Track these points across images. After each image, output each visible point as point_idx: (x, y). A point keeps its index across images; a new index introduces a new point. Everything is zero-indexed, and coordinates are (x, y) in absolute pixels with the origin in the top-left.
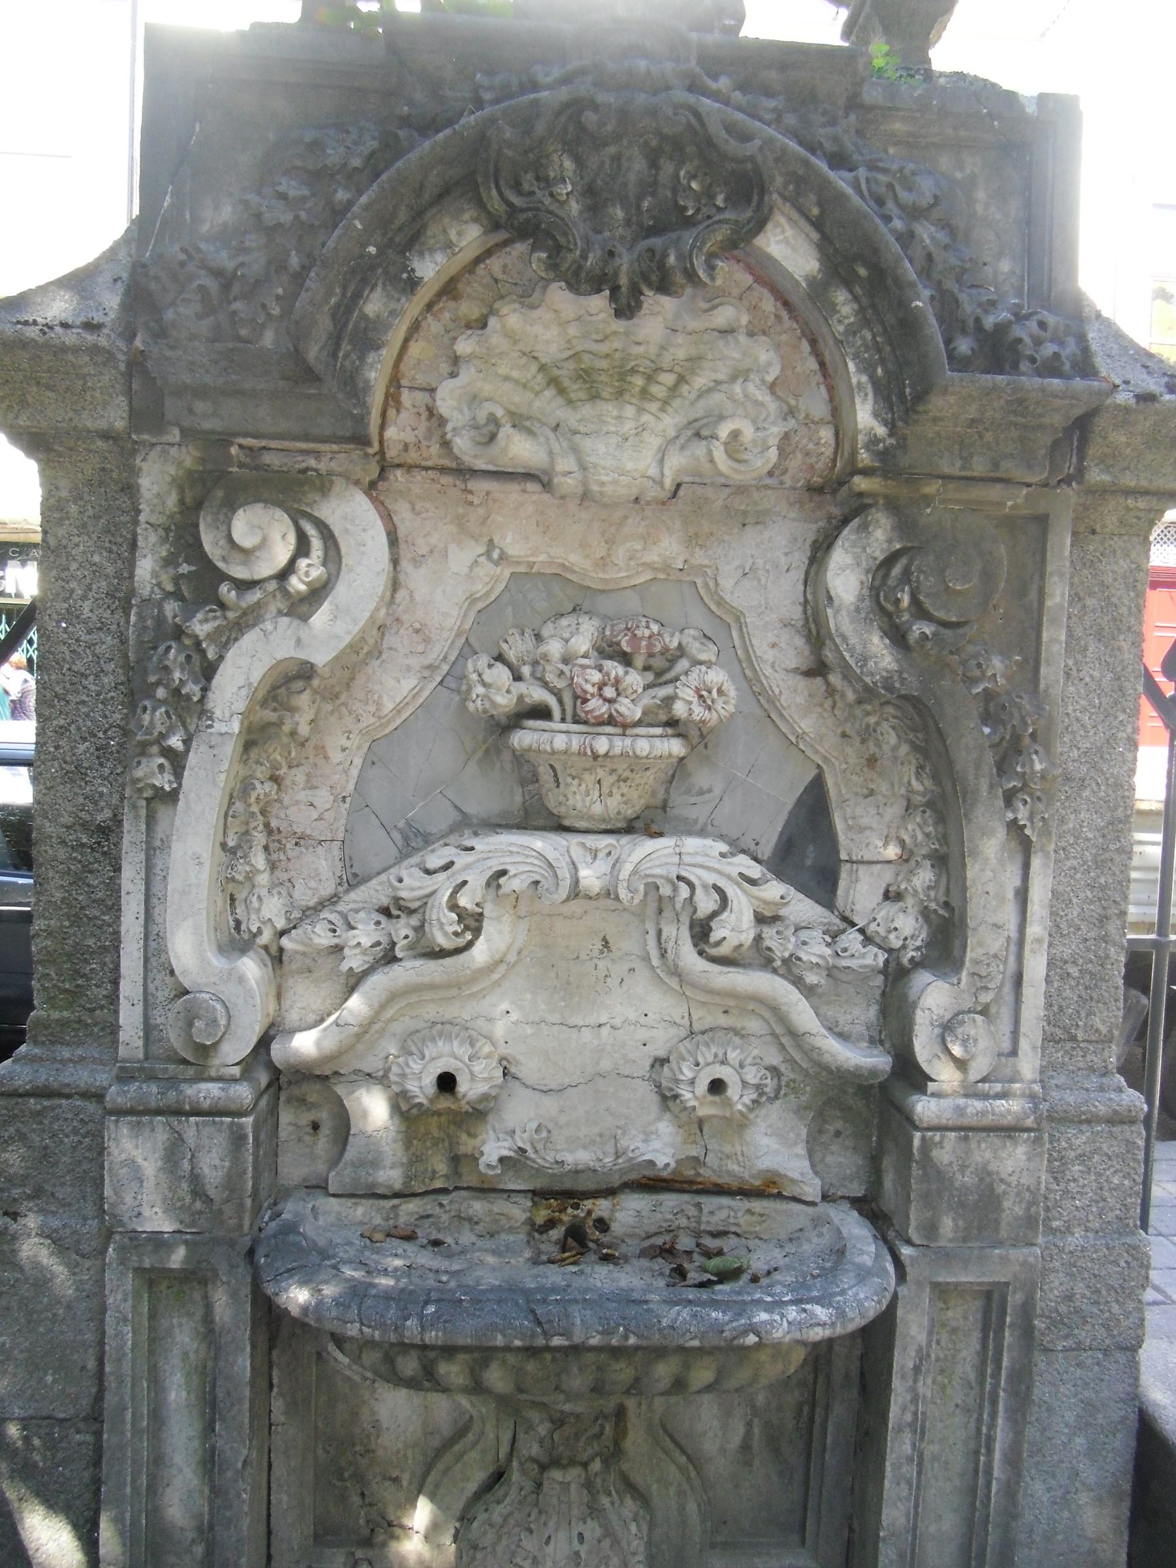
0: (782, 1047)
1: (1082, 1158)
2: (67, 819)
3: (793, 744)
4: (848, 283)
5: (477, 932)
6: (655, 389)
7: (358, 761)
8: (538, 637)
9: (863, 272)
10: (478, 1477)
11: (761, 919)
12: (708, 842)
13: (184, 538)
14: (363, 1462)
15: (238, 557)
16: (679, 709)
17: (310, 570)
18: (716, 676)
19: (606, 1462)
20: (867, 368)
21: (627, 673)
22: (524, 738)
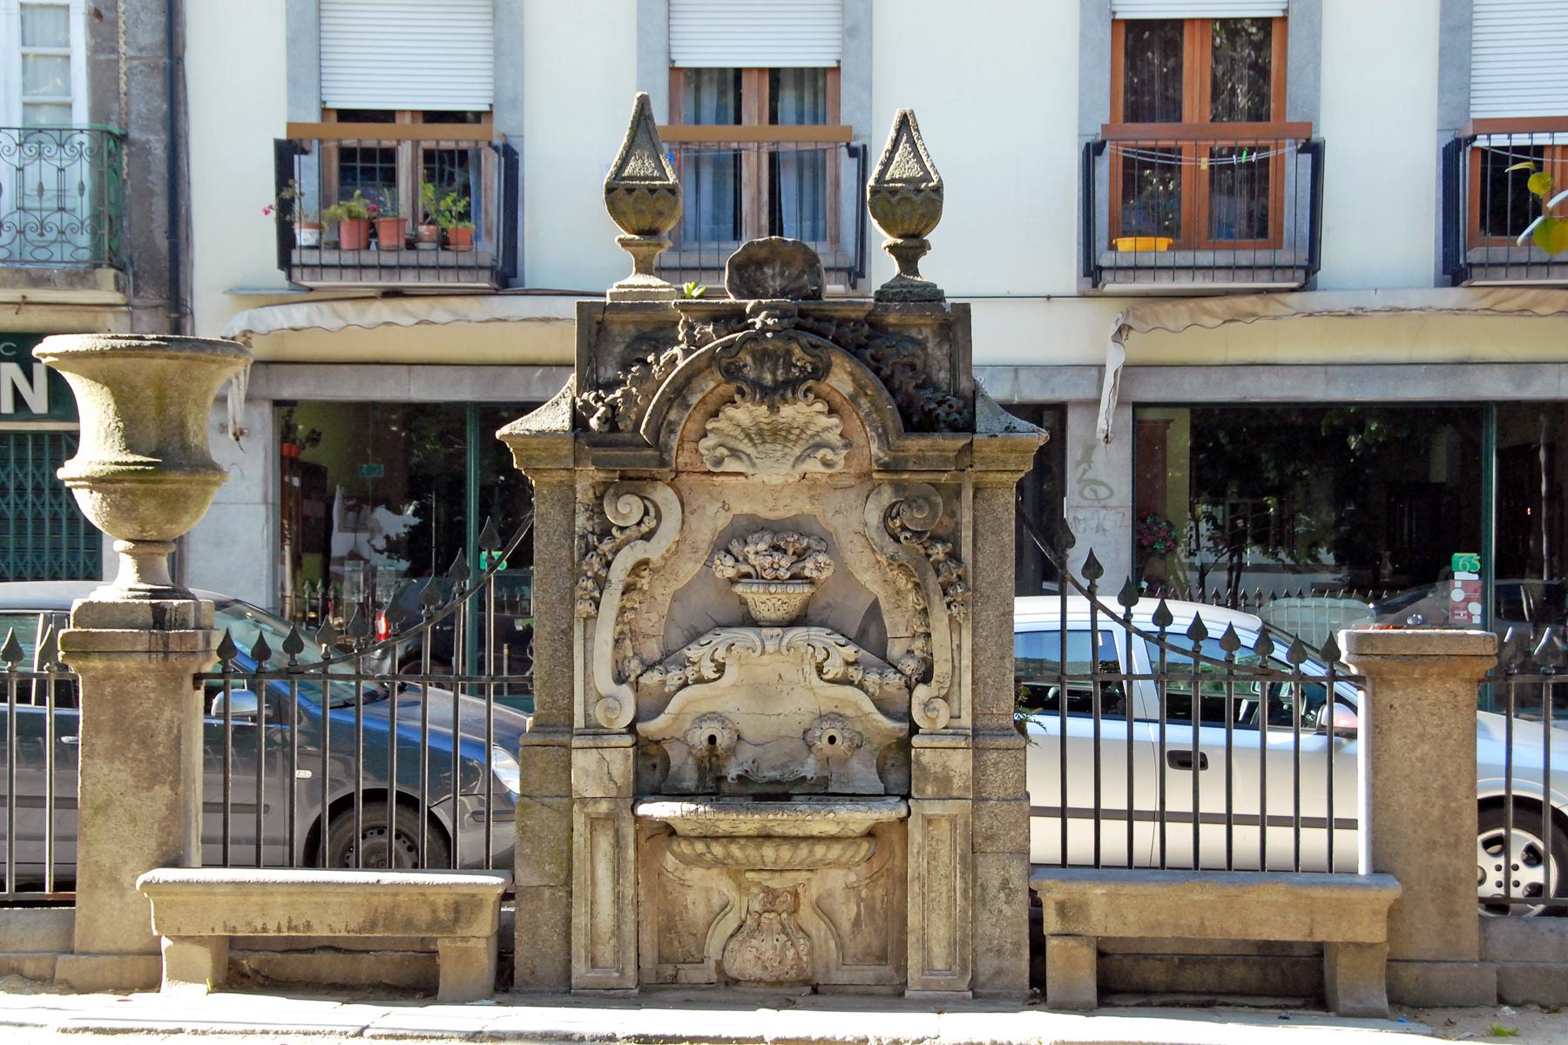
13: (597, 510)
17: (649, 523)
19: (790, 914)
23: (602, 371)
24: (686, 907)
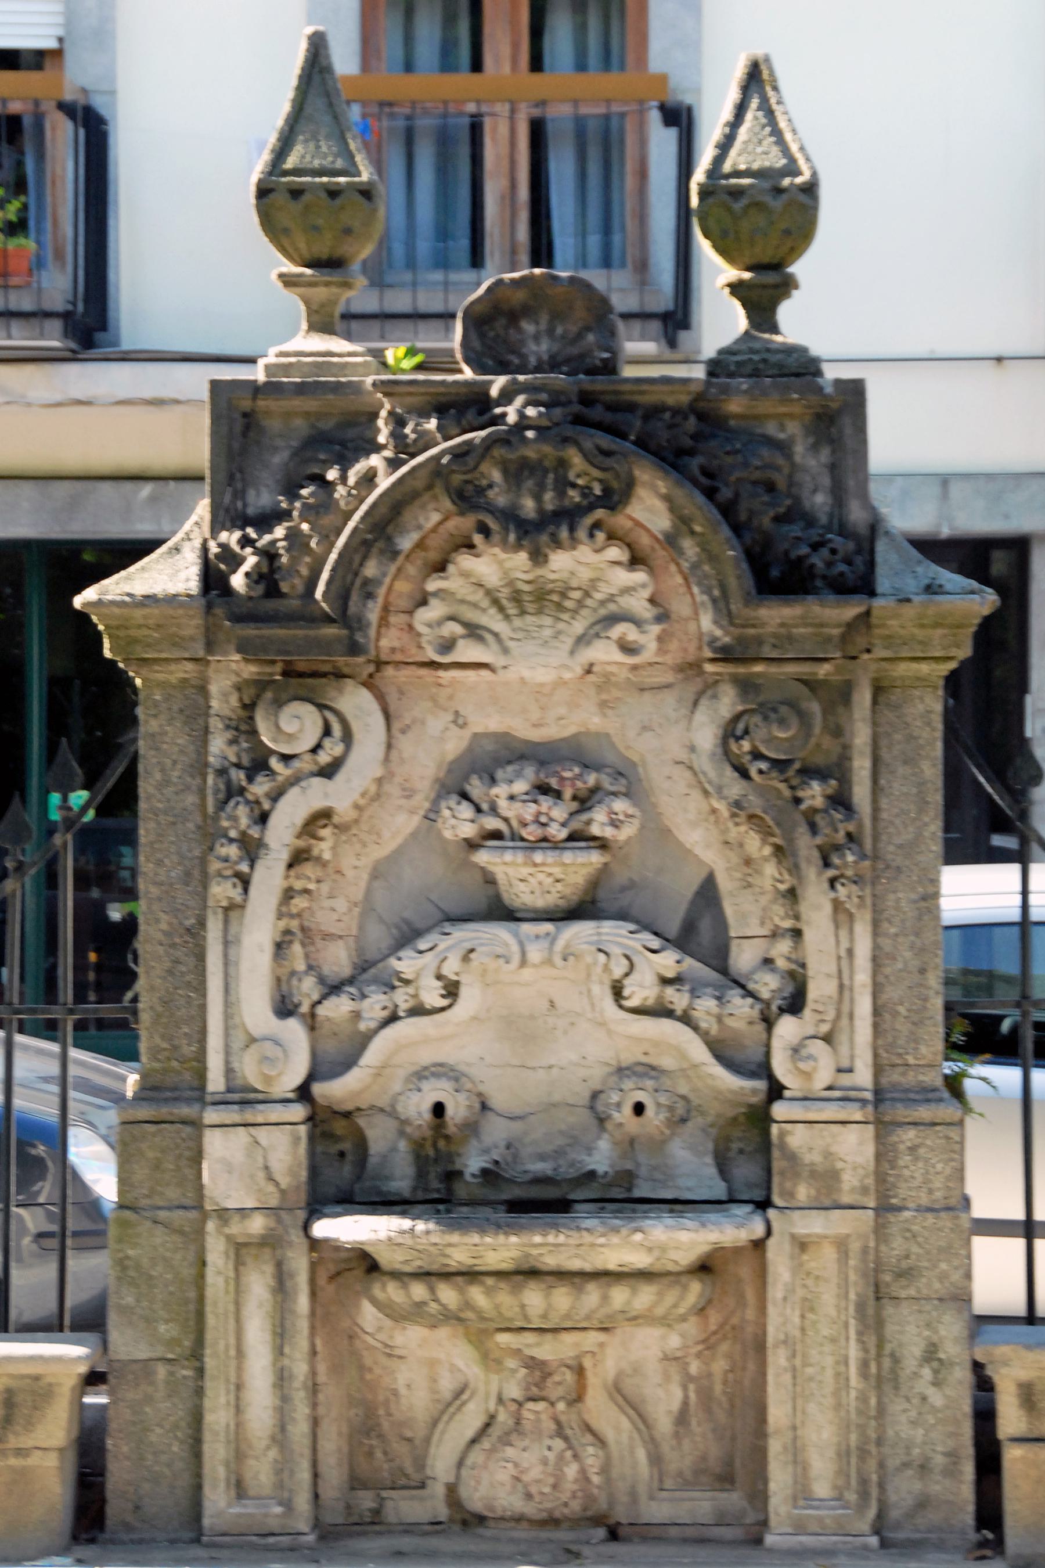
13: (244, 728)
17: (333, 749)
21: (316, 763)
23: (251, 495)
24: (395, 1393)
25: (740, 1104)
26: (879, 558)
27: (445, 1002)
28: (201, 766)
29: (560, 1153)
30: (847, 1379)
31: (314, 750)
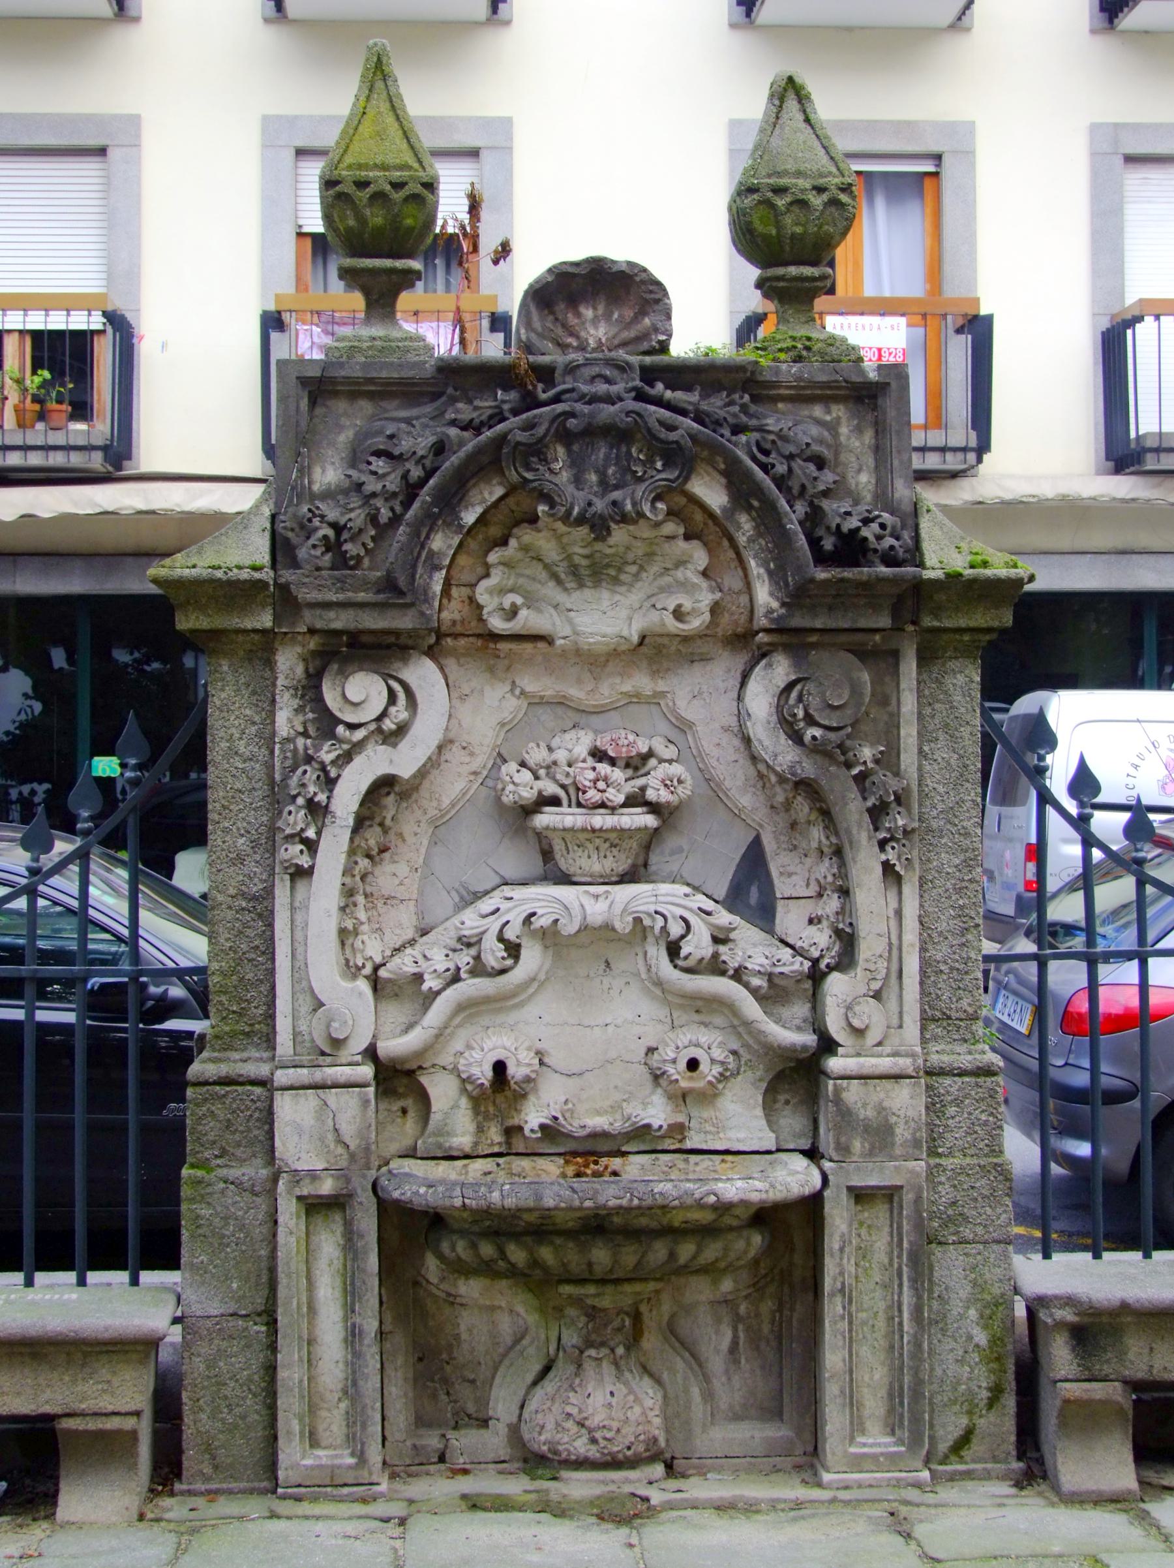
0: (739, 1035)
1: (957, 1102)
2: (232, 891)
3: (737, 815)
4: (749, 508)
5: (516, 957)
6: (623, 577)
7: (425, 842)
8: (550, 749)
9: (756, 503)
10: (537, 1367)
11: (716, 940)
12: (676, 886)
14: (448, 1368)
15: (348, 707)
16: (651, 795)
17: (399, 712)
18: (676, 769)
19: (628, 1348)
20: (765, 564)
22: (546, 819)
23: (317, 472)
24: (457, 1337)
25: (790, 1059)
26: (924, 534)
27: (509, 962)
28: (268, 738)
29: (616, 1107)
30: (901, 1324)
31: (380, 718)
